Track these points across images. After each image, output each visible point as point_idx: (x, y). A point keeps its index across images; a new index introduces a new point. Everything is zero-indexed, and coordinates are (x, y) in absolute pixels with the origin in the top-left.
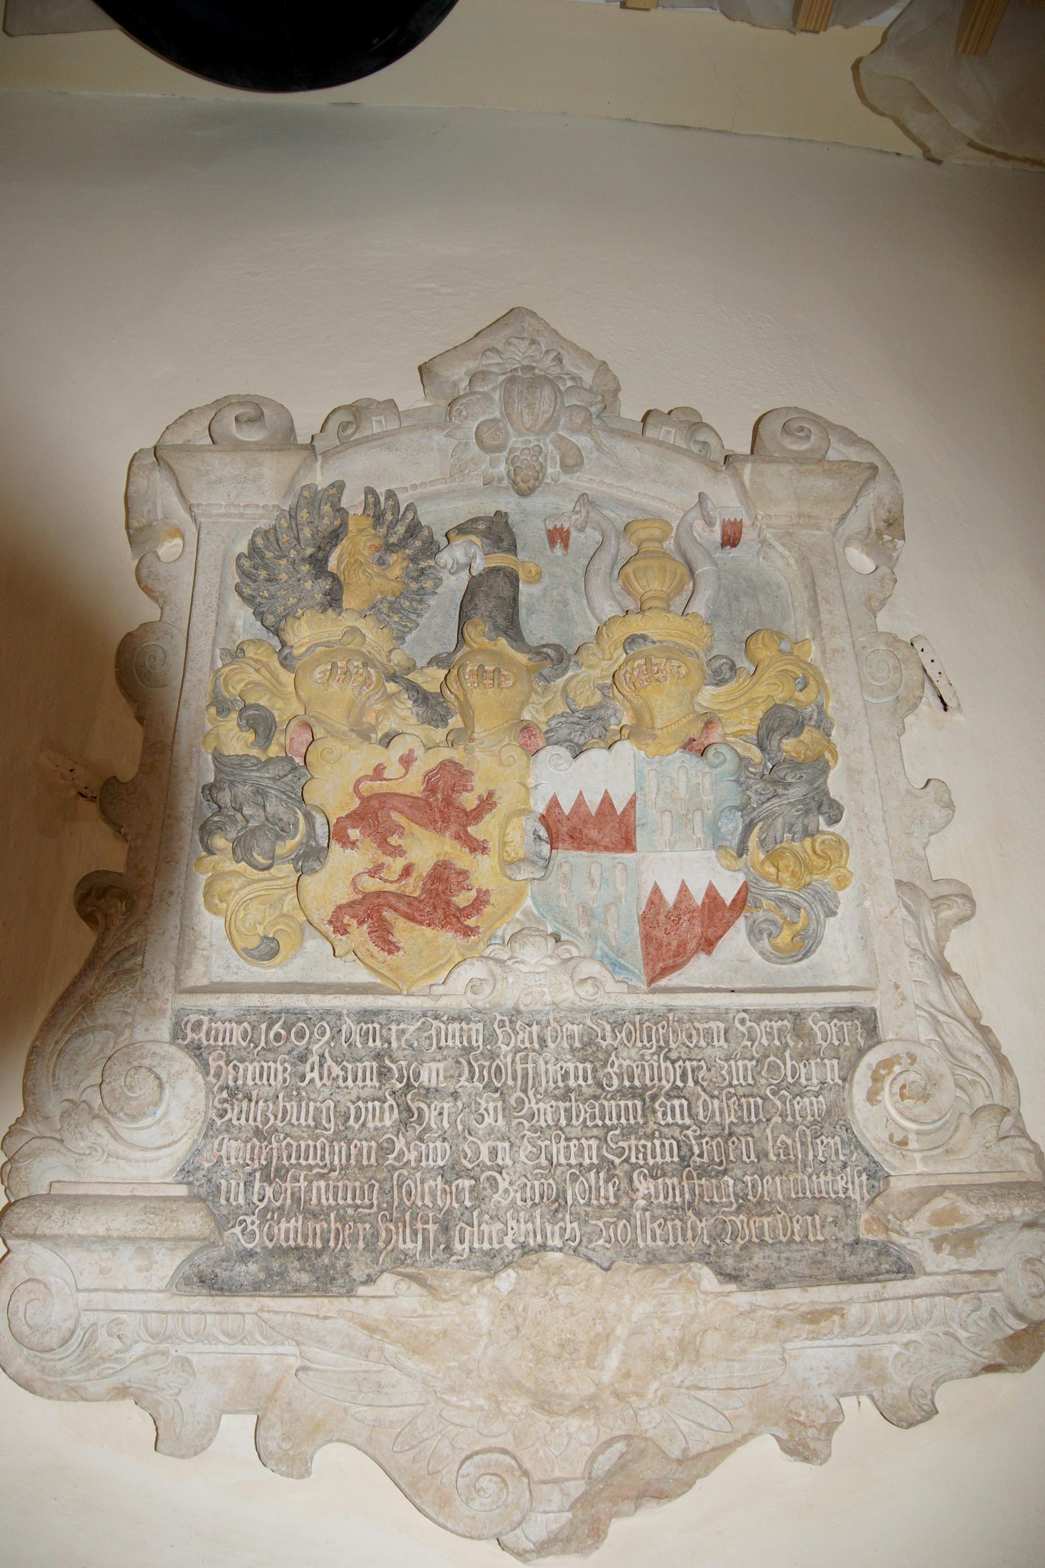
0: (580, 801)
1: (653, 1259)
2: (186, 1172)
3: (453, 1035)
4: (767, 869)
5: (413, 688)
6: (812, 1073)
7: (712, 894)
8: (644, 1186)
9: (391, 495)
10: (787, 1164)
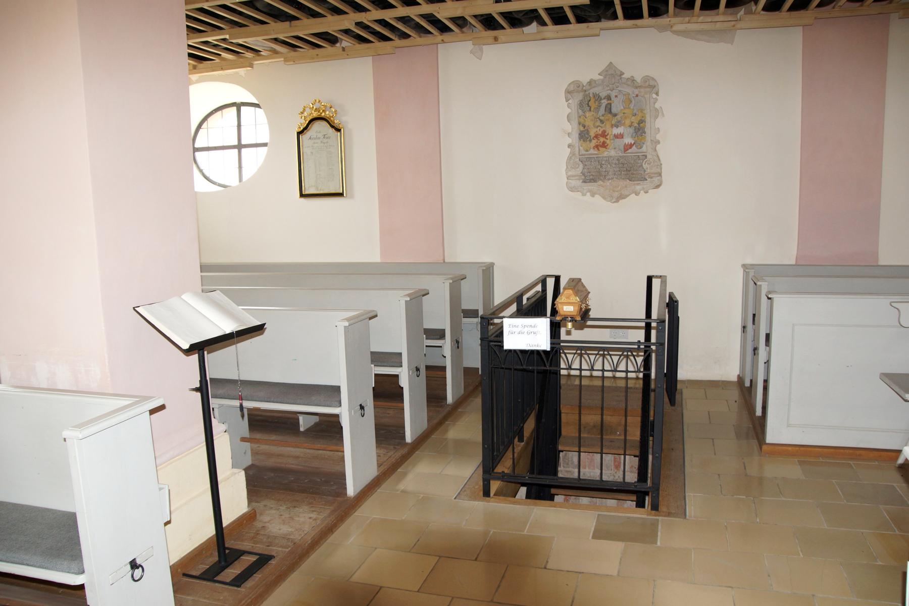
0: (628, 143)
1: (623, 179)
2: (582, 173)
3: (605, 159)
4: (248, 586)
5: (600, 120)
6: (639, 162)
7: (631, 143)
8: (623, 172)
9: (596, 93)
10: (636, 170)
